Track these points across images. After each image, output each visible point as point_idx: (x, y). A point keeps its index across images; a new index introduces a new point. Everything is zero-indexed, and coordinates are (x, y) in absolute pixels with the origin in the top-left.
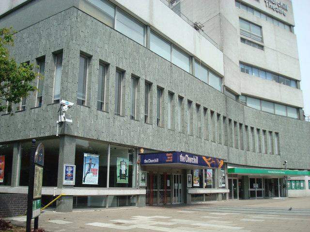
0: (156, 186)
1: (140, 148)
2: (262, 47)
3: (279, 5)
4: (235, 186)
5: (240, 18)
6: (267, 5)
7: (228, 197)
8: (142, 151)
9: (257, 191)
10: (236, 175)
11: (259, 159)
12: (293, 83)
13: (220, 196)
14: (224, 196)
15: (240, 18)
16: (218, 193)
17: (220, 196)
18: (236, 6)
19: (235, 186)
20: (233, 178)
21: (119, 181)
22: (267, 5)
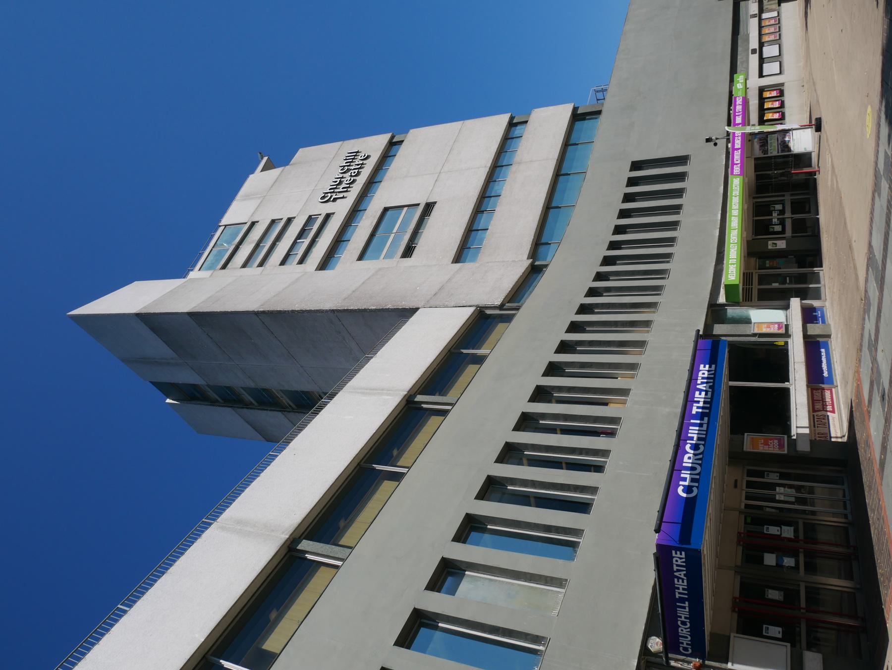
0: (762, 100)
1: (644, 650)
2: (429, 207)
3: (345, 170)
4: (782, 278)
5: (458, 258)
6: (341, 195)
7: (816, 303)
8: (656, 644)
9: (793, 213)
10: (746, 277)
11: (713, 227)
12: (518, 131)
13: (814, 329)
14: (809, 316)
15: (361, 258)
16: (806, 337)
17: (814, 329)
18: (333, 269)
19: (782, 278)
20: (756, 287)
21: (769, 116)
22: (341, 195)
